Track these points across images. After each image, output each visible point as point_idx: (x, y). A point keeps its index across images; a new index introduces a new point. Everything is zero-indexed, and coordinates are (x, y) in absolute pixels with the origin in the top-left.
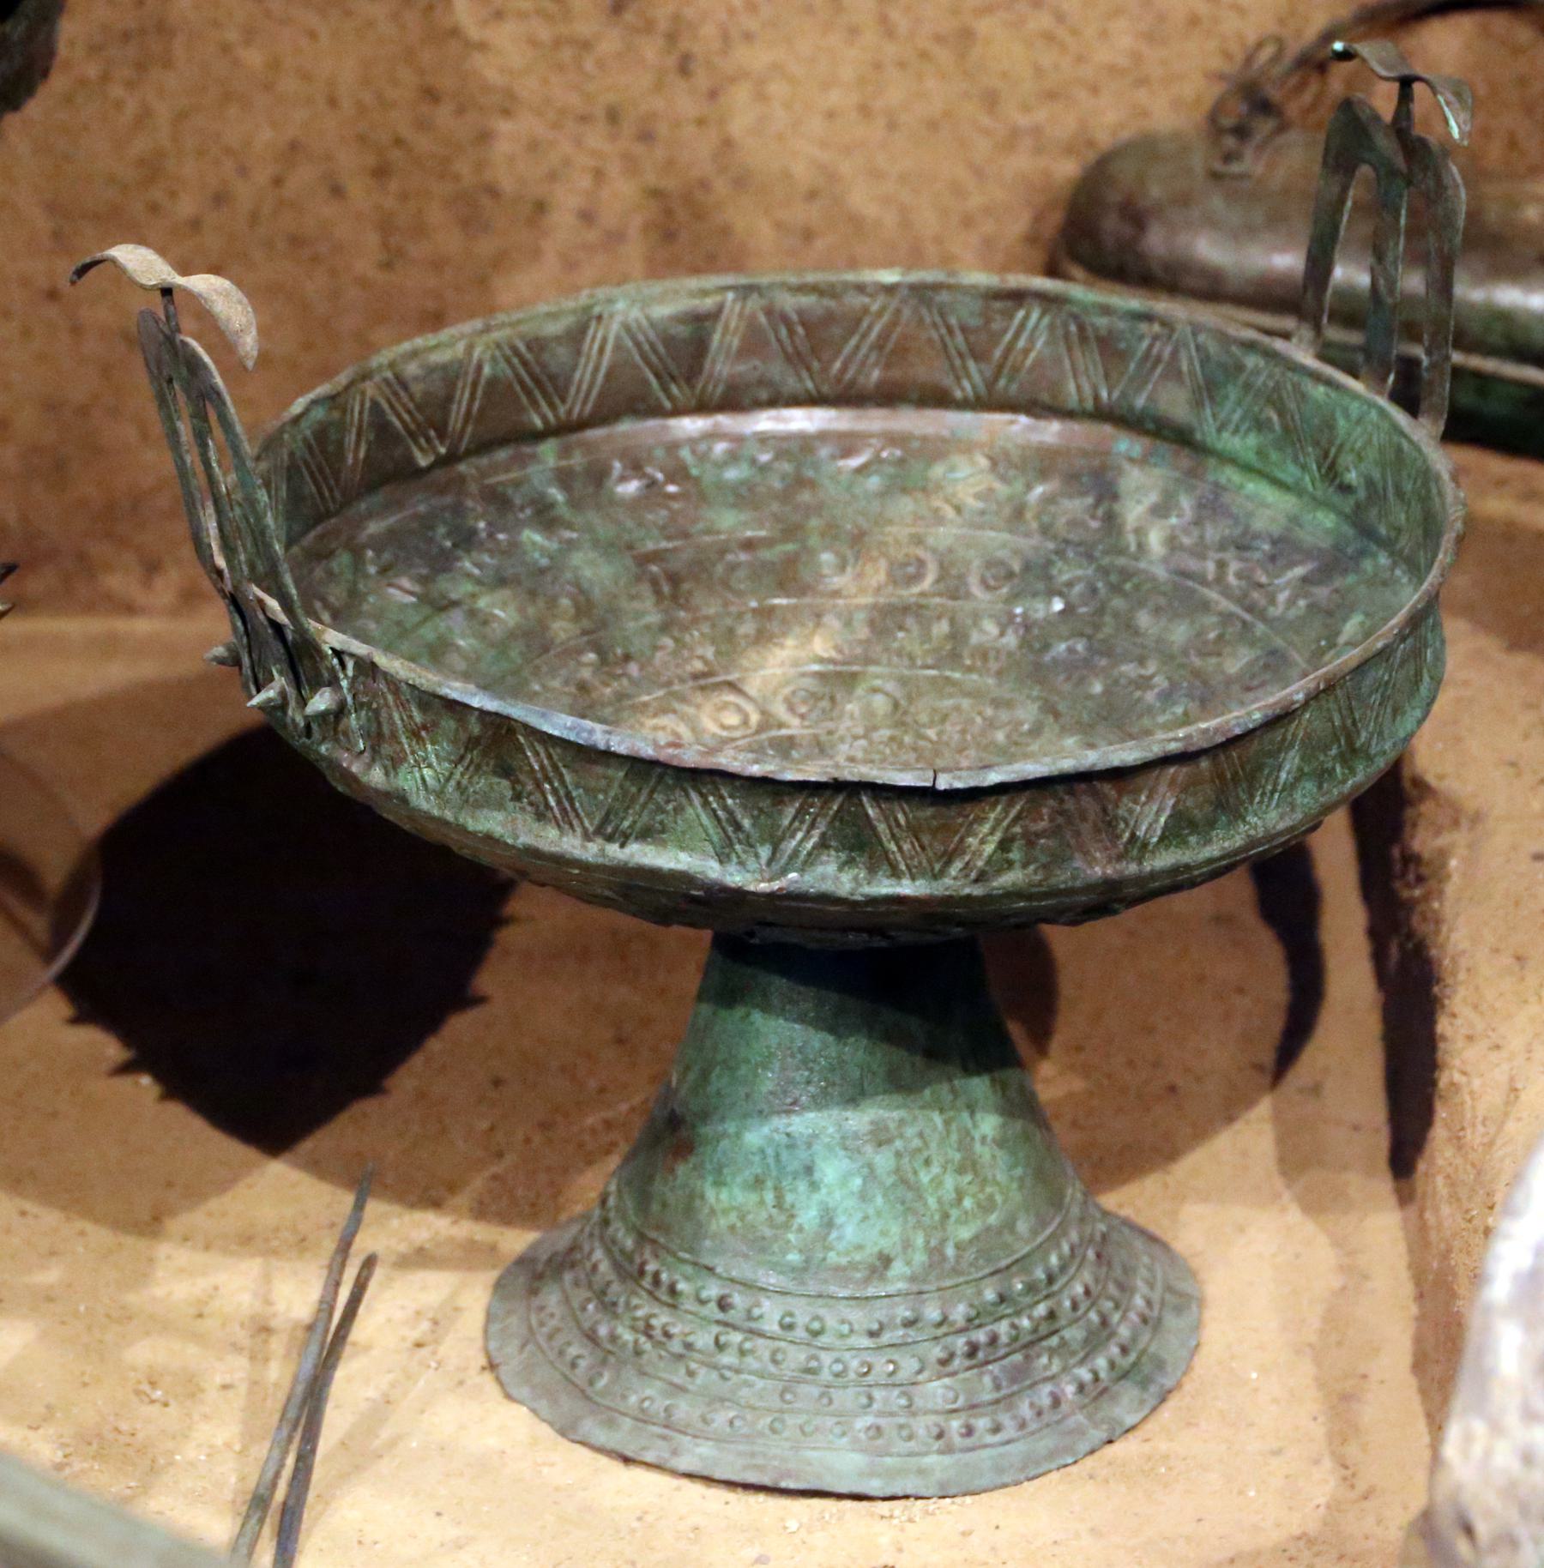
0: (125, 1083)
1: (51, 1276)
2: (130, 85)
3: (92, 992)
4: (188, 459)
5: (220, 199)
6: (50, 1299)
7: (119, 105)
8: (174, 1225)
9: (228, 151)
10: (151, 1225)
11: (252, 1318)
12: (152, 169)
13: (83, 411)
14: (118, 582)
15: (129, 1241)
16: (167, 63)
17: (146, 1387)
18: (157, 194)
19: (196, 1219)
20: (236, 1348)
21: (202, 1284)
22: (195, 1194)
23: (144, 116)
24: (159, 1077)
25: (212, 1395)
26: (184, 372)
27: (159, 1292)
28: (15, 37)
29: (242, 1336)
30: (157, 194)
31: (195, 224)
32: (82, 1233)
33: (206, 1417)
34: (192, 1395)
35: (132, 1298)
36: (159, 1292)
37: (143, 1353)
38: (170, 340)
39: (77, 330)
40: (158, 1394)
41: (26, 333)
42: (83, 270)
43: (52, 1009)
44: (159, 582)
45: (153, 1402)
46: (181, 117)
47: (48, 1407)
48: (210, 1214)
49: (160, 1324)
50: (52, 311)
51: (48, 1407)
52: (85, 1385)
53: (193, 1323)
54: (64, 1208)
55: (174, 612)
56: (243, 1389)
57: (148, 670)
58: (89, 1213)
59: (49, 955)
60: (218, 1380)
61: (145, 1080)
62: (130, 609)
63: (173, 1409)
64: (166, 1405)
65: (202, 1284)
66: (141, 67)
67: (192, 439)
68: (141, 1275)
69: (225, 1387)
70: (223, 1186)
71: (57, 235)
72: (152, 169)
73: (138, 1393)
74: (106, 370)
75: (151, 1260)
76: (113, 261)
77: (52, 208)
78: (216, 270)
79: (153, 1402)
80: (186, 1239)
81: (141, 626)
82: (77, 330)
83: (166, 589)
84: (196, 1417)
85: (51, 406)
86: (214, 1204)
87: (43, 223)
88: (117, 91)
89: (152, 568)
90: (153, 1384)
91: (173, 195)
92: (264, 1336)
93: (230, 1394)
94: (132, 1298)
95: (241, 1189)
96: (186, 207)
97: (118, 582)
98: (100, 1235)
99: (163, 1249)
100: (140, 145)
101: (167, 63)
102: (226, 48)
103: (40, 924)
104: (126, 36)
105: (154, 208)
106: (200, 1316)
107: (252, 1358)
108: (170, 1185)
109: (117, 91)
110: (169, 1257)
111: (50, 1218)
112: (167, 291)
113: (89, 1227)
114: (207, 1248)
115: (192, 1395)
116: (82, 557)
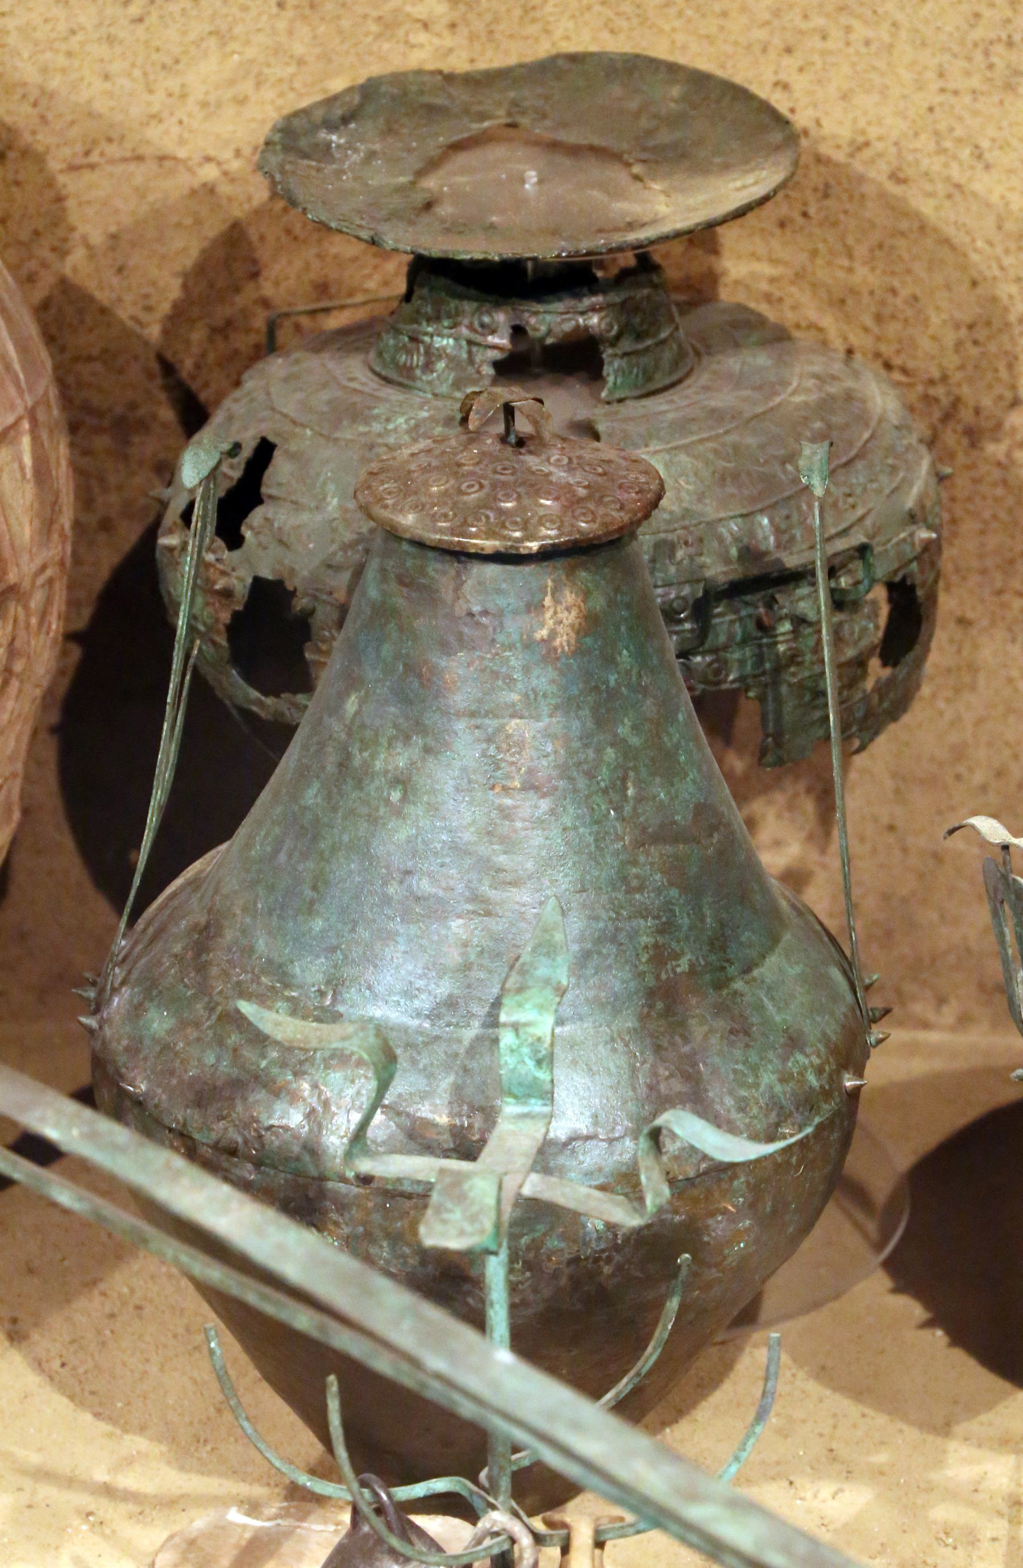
0: (926, 1334)
1: (882, 1458)
2: (948, 700)
3: (905, 1273)
4: (1010, 951)
5: (1000, 773)
6: (882, 1473)
7: (941, 713)
8: (959, 1429)
9: (1007, 744)
10: (944, 1429)
11: (1010, 1496)
12: (959, 753)
13: (904, 901)
14: (920, 1009)
15: (930, 1438)
16: (973, 687)
17: (943, 1536)
18: (961, 769)
19: (974, 1426)
20: (1000, 1514)
21: (976, 1470)
22: (972, 1409)
23: (957, 721)
24: (948, 1332)
25: (985, 1545)
26: (1013, 897)
27: (949, 1473)
28: (900, 677)
29: (1003, 1507)
30: (961, 769)
31: (984, 788)
32: (901, 1431)
33: (981, 1558)
34: (972, 1543)
35: (934, 1476)
36: (949, 1473)
37: (941, 1513)
38: (1005, 877)
39: (905, 850)
40: (950, 1541)
41: (874, 851)
42: (951, 832)
43: (880, 1282)
44: (945, 1009)
45: (947, 1545)
46: (979, 722)
47: (882, 1545)
48: (982, 1424)
49: (951, 1494)
50: (891, 839)
51: (882, 1545)
52: (905, 1532)
53: (971, 1494)
54: (889, 1414)
55: (953, 1029)
56: (1004, 1542)
57: (938, 1065)
58: (905, 1418)
59: (879, 1247)
60: (989, 1535)
61: (939, 1333)
62: (926, 1025)
63: (961, 1552)
64: (955, 1548)
65: (976, 1470)
66: (957, 691)
67: (1014, 941)
68: (939, 1463)
69: (994, 1539)
70: (989, 1406)
71: (897, 791)
72: (959, 753)
73: (937, 1539)
74: (921, 876)
75: (944, 1452)
76: (973, 827)
77: (894, 775)
78: (994, 816)
79: (947, 1545)
80: (966, 1439)
81: (934, 1037)
82: (905, 850)
83: (949, 1014)
84: (975, 1558)
85: (886, 897)
86: (983, 1417)
87: (889, 784)
88: (941, 704)
89: (941, 1001)
90: (947, 1534)
91: (971, 769)
92: (1017, 1507)
93: (996, 1544)
94: (934, 1476)
95: (1000, 1408)
96: (979, 777)
97: (920, 1009)
98: (912, 1433)
99: (952, 1445)
100: (954, 738)
101: (973, 687)
102: (1010, 680)
103: (872, 1227)
104: (949, 671)
105: (958, 777)
106: (976, 1491)
107: (1010, 1522)
108: (956, 1402)
109: (941, 704)
110: (956, 1451)
111: (882, 1420)
112: (1006, 847)
113: (905, 1427)
114: (980, 1446)
115: (972, 1543)
116: (898, 992)
